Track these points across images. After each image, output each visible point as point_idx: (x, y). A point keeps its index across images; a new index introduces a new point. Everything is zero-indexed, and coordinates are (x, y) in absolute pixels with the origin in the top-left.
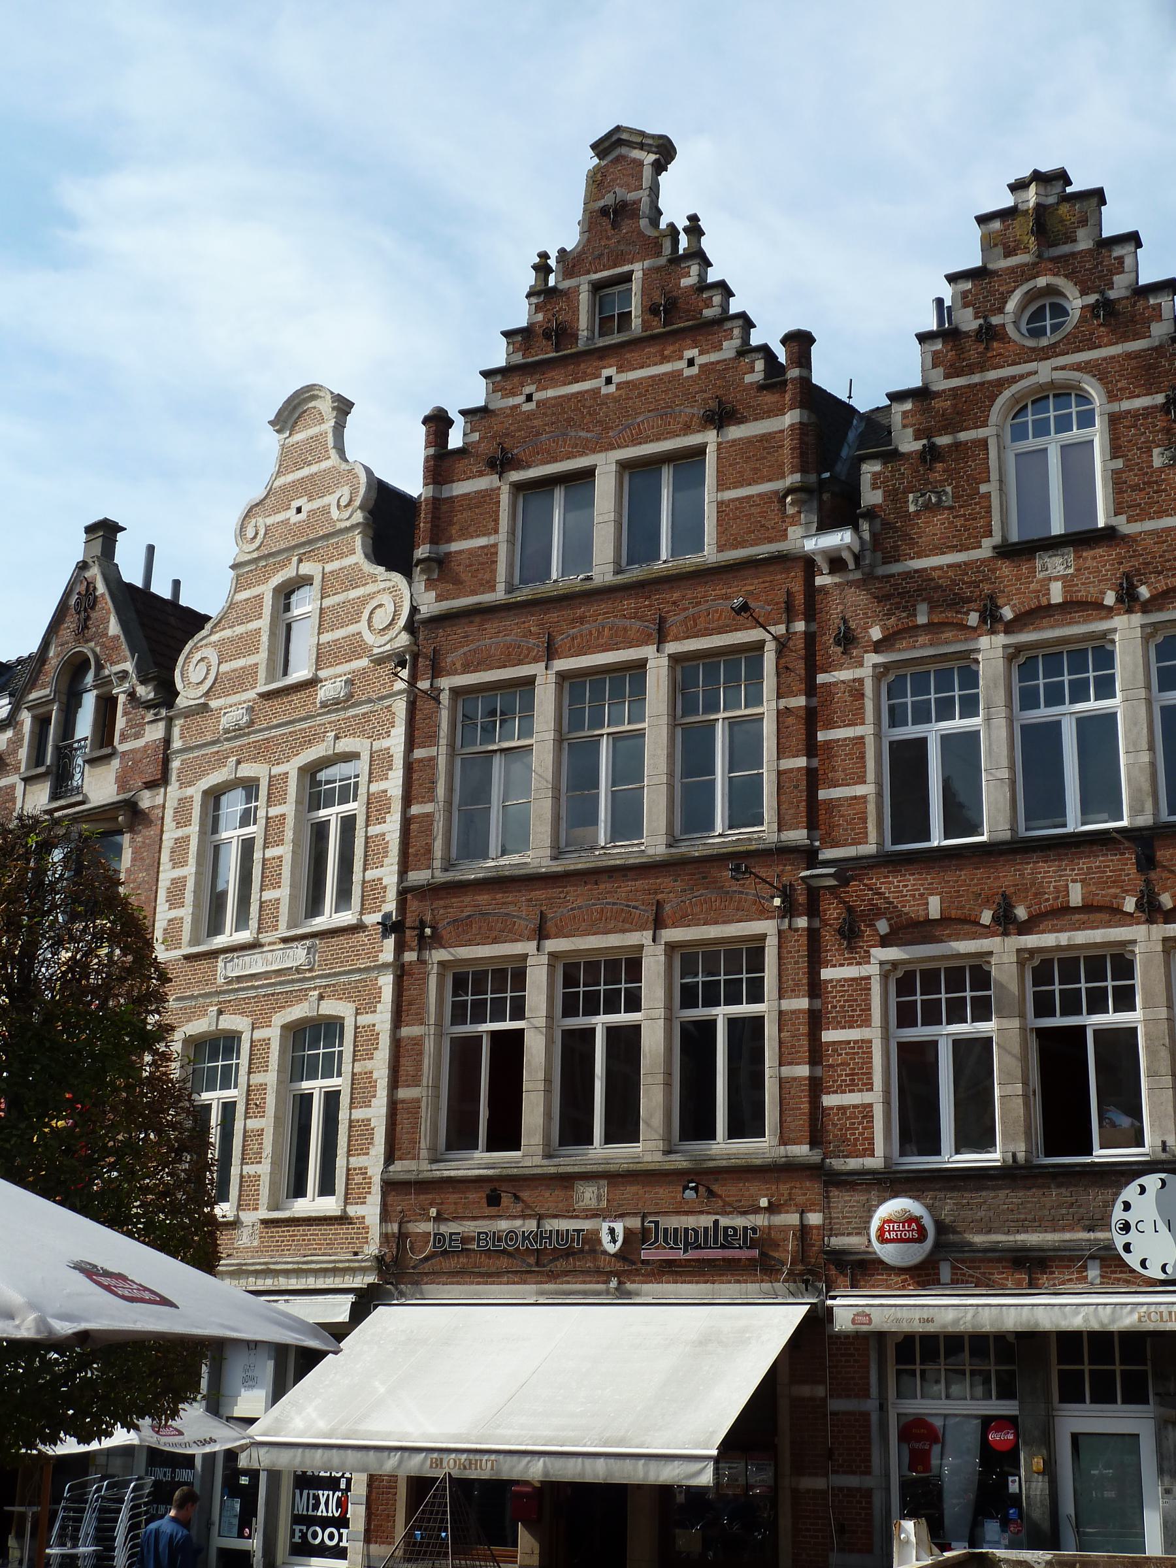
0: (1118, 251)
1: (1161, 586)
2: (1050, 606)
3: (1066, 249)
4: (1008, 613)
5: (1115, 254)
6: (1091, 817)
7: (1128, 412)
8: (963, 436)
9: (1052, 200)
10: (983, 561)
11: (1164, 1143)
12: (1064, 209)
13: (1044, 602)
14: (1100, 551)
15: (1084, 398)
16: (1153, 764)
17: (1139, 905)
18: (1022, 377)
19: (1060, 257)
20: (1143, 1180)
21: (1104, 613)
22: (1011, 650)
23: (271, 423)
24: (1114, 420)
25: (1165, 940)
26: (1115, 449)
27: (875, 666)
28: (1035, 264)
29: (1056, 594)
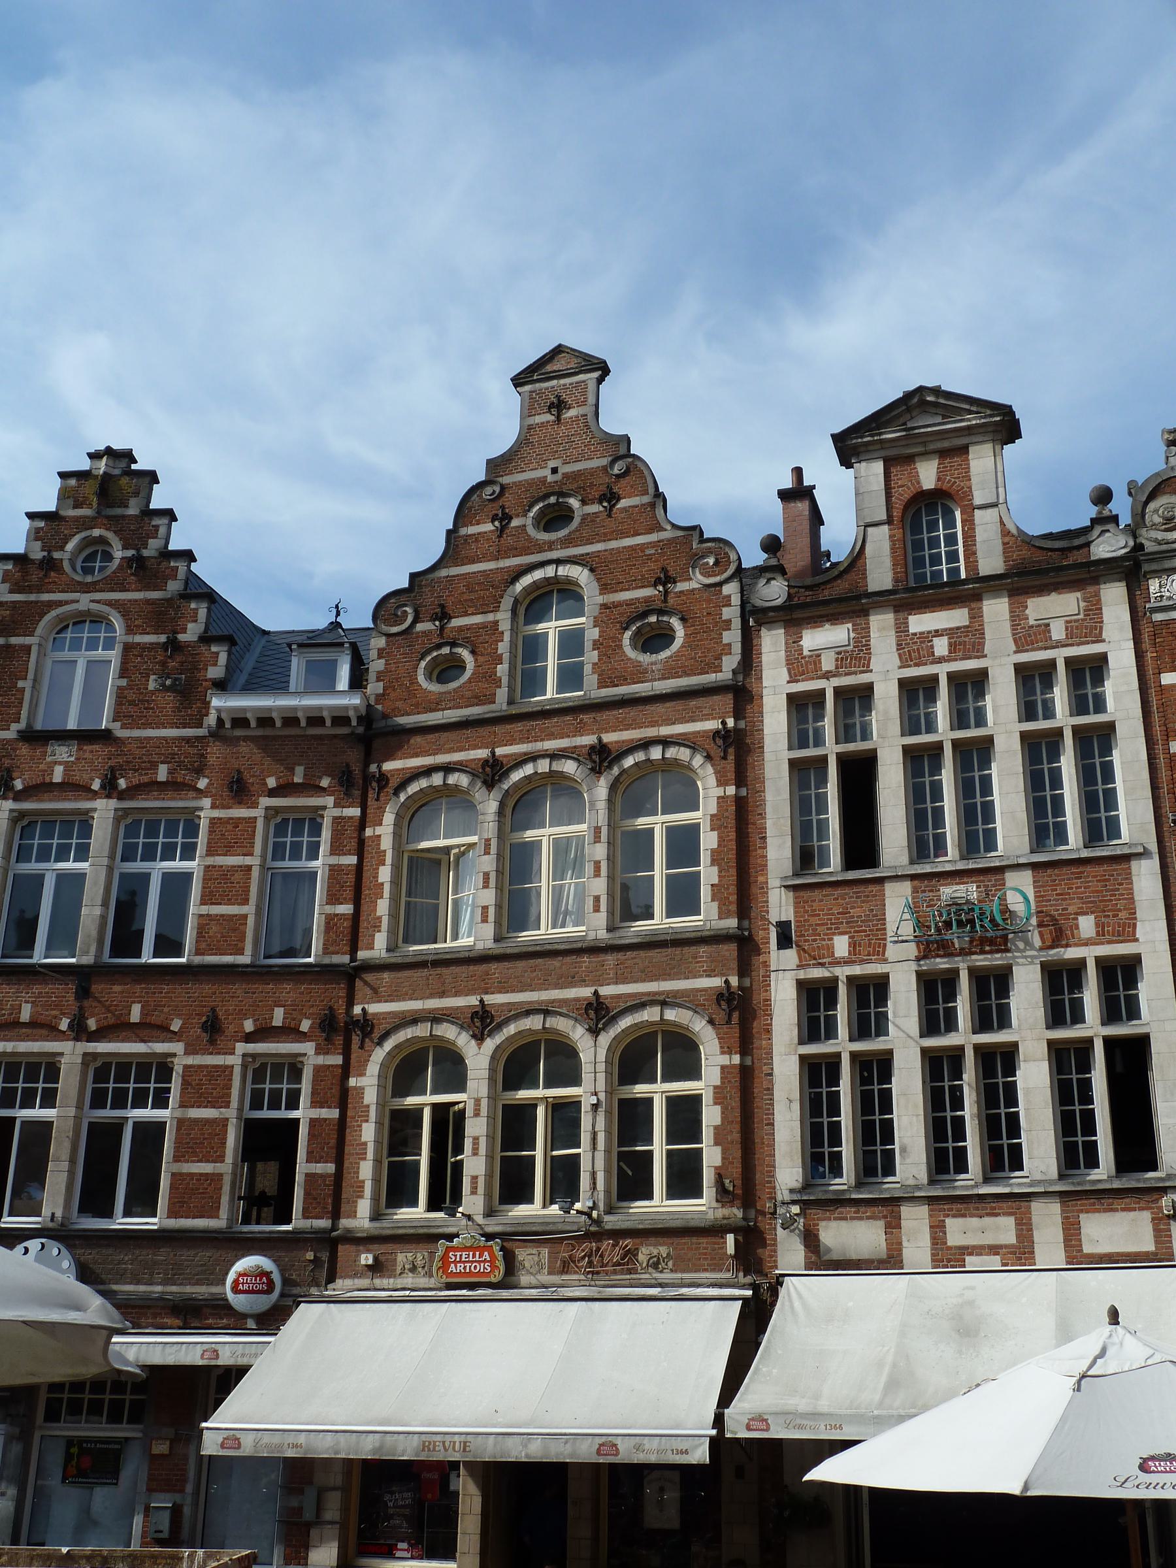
0: (156, 521)
1: (135, 781)
2: (52, 784)
3: (119, 511)
4: (18, 785)
5: (154, 523)
6: (52, 953)
7: (139, 644)
8: (14, 640)
9: (117, 472)
10: (8, 741)
11: (53, 1214)
12: (125, 480)
13: (47, 780)
14: (96, 747)
15: (110, 625)
16: (103, 918)
17: (70, 1026)
18: (67, 603)
19: (115, 516)
20: (27, 1244)
21: (90, 795)
22: (15, 814)
23: (814, 487)
24: (127, 648)
25: (85, 1055)
26: (123, 672)
27: (267, 808)
28: (94, 518)
29: (58, 775)
